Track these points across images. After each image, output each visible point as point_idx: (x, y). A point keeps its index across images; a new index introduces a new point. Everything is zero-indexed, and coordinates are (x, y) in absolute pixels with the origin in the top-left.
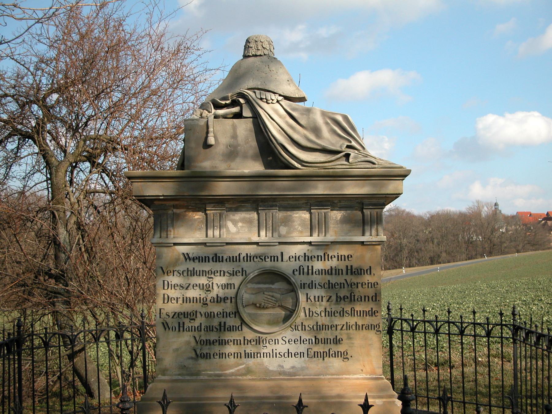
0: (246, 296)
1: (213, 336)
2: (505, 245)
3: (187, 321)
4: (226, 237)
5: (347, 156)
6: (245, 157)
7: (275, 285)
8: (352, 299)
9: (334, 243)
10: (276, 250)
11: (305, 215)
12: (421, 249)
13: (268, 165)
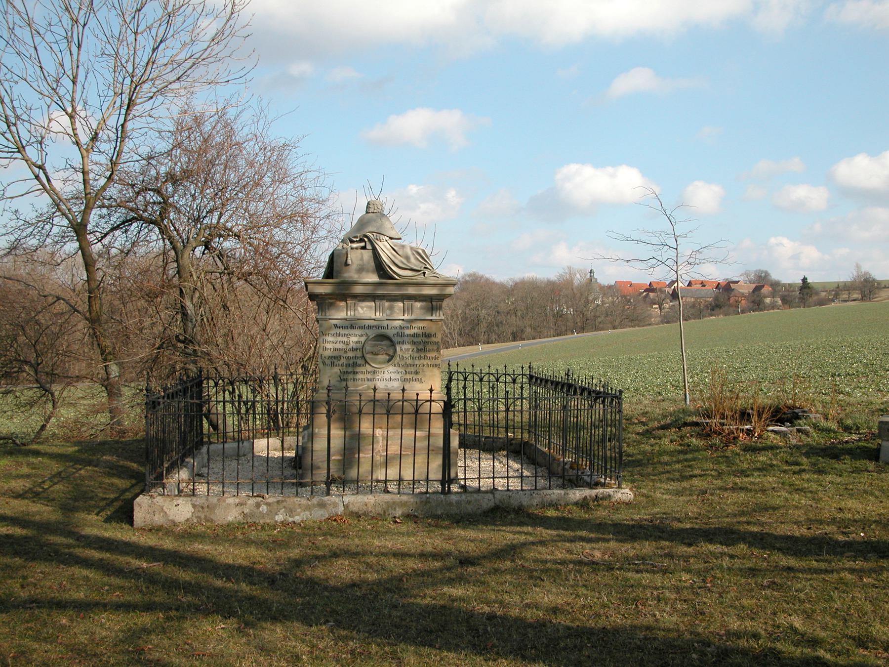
0: (368, 348)
1: (350, 369)
2: (599, 320)
3: (336, 361)
4: (358, 316)
5: (424, 273)
6: (368, 271)
7: (385, 341)
8: (424, 350)
9: (416, 320)
10: (385, 323)
11: (401, 304)
12: (501, 323)
13: (380, 277)
